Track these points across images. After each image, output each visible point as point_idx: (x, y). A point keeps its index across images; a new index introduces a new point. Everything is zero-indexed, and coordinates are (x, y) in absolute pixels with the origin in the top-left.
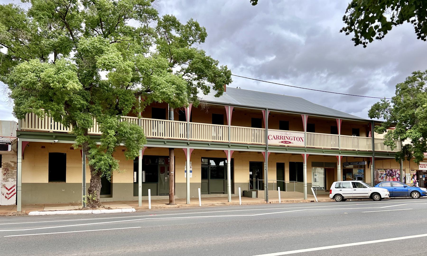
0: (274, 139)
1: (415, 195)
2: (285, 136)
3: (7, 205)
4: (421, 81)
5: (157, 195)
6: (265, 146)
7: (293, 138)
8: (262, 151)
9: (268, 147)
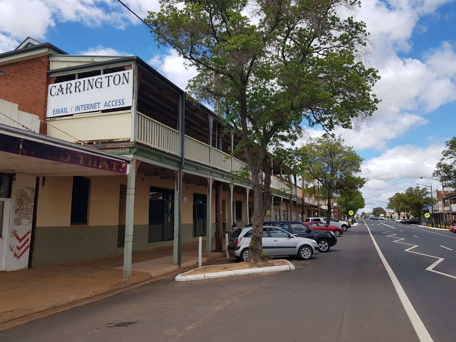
5: (163, 241)
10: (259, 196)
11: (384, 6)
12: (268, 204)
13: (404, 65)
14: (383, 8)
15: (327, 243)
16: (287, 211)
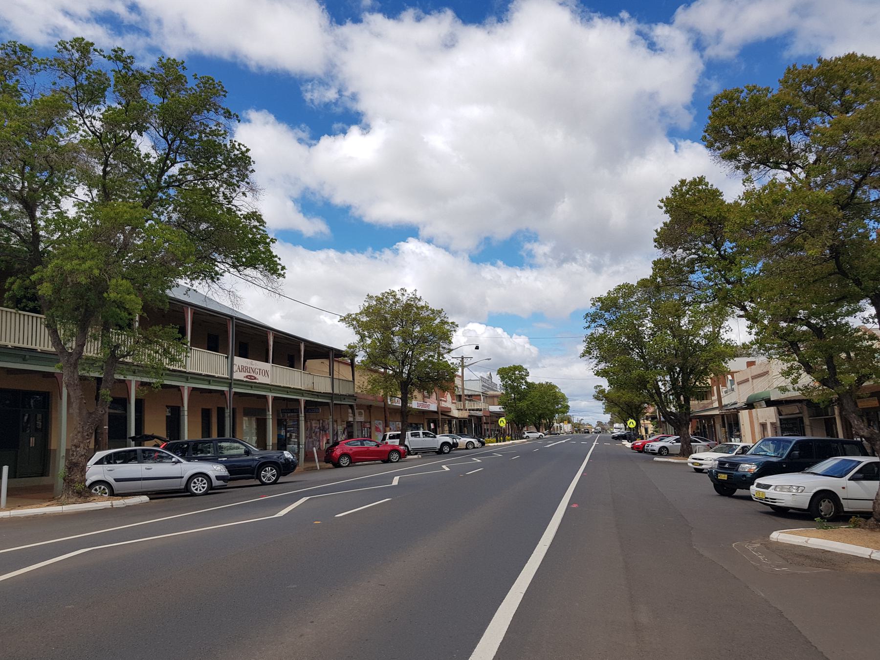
0: (238, 371)
1: (395, 456)
2: (251, 366)
3: (502, 640)
4: (45, 284)
5: (15, 477)
6: (230, 381)
7: (258, 371)
8: (225, 389)
9: (233, 382)
10: (78, 401)
11: (644, 46)
12: (101, 413)
13: (676, 151)
14: (642, 49)
15: (274, 471)
16: (370, 422)
